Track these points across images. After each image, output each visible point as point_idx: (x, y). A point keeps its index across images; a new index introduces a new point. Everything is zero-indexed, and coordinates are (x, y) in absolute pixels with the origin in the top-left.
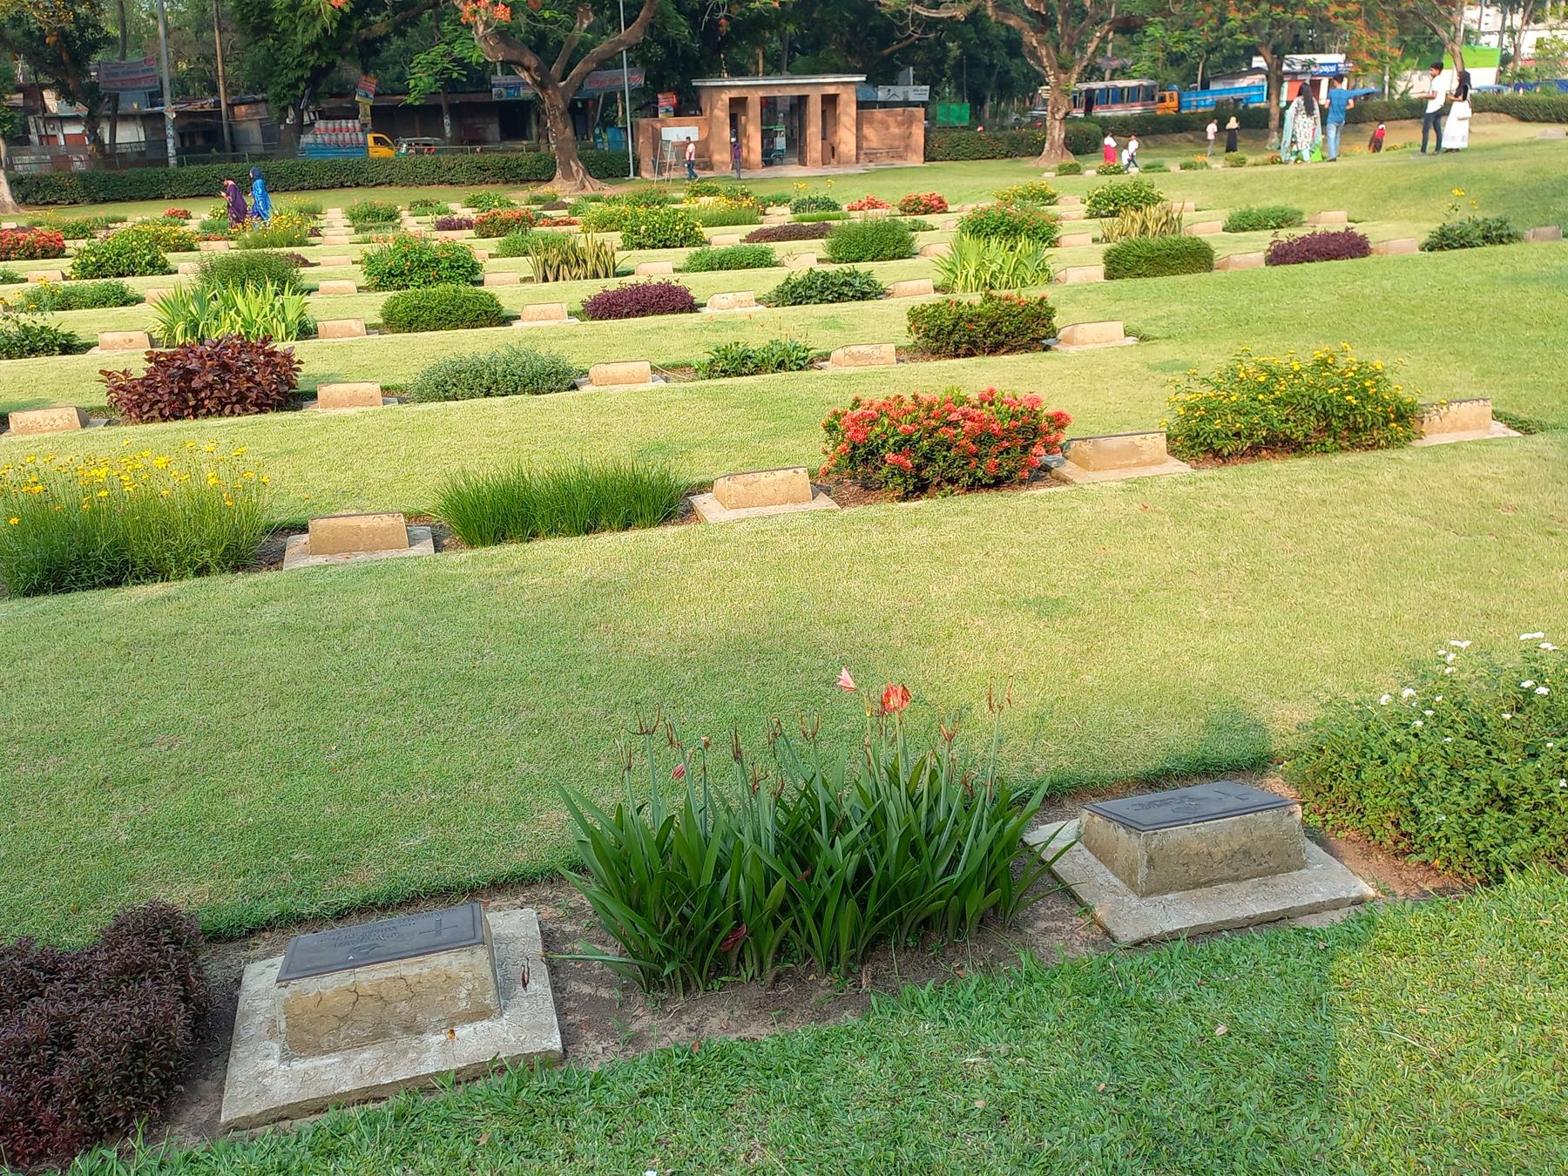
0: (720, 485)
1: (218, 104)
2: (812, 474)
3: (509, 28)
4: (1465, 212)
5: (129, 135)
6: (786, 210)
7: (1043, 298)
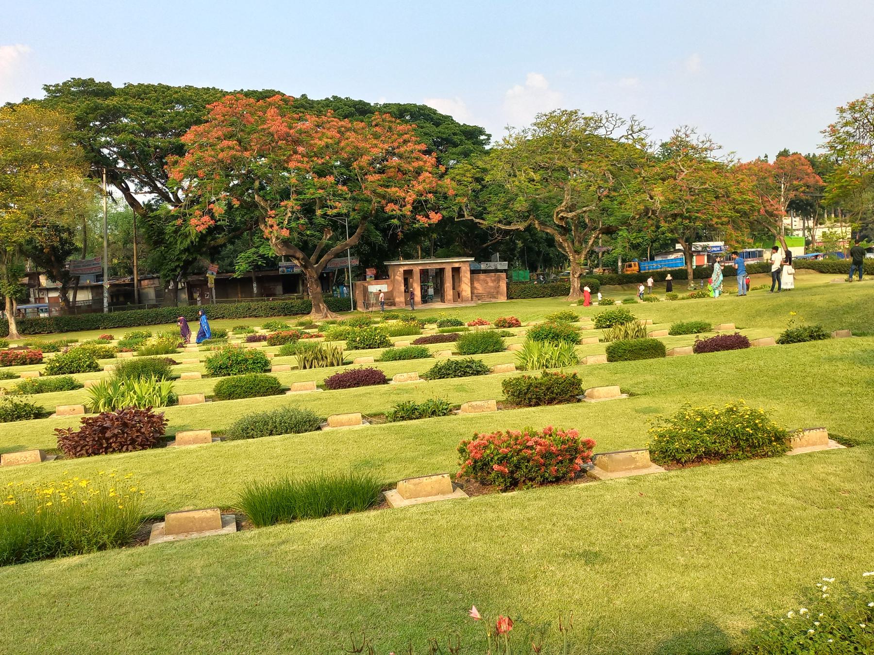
0: (401, 484)
1: (133, 279)
2: (452, 477)
3: (288, 239)
4: (799, 323)
5: (84, 297)
6: (435, 326)
7: (575, 374)
